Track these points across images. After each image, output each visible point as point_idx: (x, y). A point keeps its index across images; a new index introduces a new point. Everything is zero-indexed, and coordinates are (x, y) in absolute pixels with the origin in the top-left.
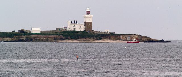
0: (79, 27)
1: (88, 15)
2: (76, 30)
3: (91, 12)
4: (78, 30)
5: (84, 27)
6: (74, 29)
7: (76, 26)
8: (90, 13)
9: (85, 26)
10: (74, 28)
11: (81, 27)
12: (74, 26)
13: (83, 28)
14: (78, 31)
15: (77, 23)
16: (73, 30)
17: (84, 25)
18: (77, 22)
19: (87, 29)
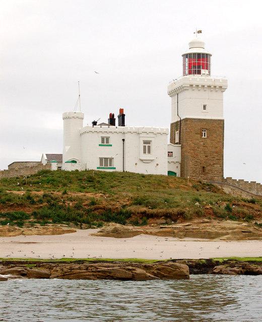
0: (134, 147)
1: (197, 76)
2: (119, 169)
3: (213, 61)
4: (132, 167)
5: (170, 154)
6: (106, 161)
7: (115, 140)
8: (207, 67)
9: (177, 150)
10: (106, 152)
11: (147, 148)
12: (105, 142)
13: (166, 158)
14: (131, 175)
15: (122, 123)
16: (93, 165)
17: (172, 140)
18: (122, 117)
19: (190, 164)
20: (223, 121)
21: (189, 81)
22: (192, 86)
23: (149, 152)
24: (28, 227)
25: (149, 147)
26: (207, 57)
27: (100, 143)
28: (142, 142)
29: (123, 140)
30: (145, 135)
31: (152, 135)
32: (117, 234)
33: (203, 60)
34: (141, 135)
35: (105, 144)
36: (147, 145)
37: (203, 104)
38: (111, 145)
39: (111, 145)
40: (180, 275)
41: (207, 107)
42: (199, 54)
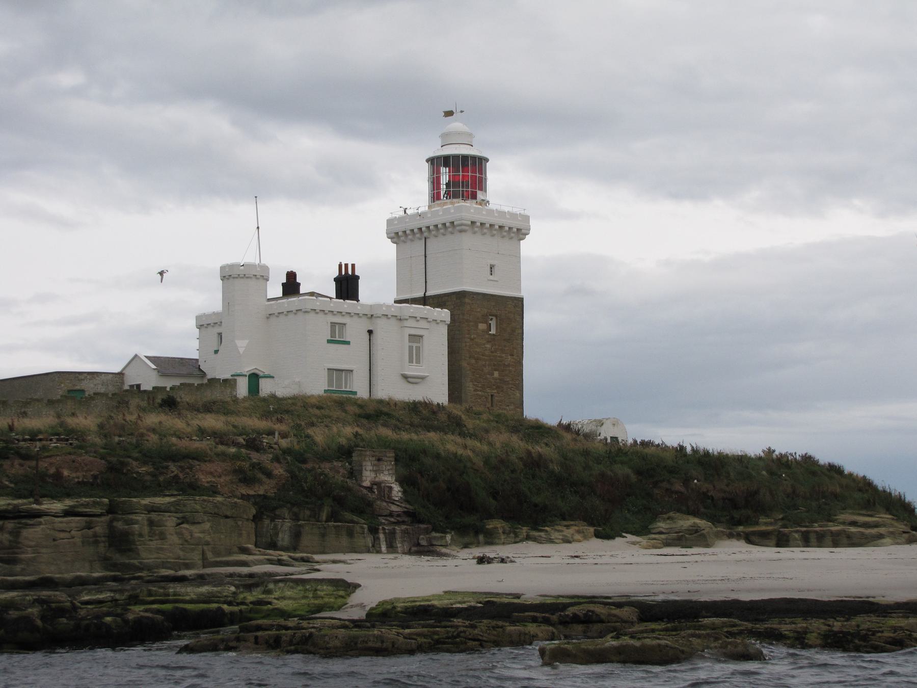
7: (355, 331)
10: (339, 357)
12: (337, 339)
20: (521, 300)
21: (406, 222)
22: (473, 223)
23: (418, 361)
24: (142, 492)
25: (418, 349)
26: (481, 164)
27: (330, 338)
28: (407, 338)
29: (370, 332)
30: (411, 323)
31: (423, 324)
32: (683, 540)
33: (474, 171)
34: (406, 323)
35: (337, 339)
36: (415, 345)
37: (493, 262)
38: (348, 343)
39: (348, 343)
40: (748, 673)
41: (496, 270)
42: (465, 158)
